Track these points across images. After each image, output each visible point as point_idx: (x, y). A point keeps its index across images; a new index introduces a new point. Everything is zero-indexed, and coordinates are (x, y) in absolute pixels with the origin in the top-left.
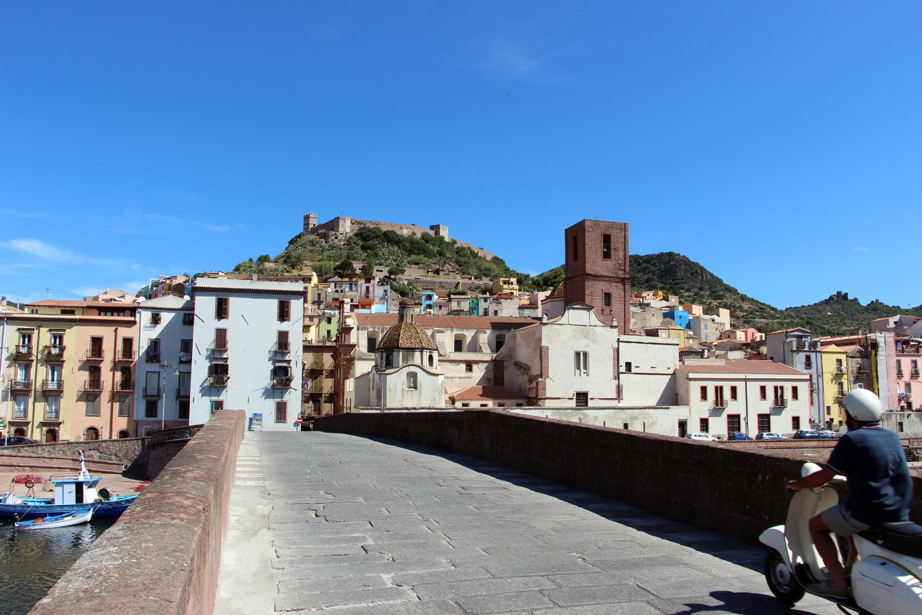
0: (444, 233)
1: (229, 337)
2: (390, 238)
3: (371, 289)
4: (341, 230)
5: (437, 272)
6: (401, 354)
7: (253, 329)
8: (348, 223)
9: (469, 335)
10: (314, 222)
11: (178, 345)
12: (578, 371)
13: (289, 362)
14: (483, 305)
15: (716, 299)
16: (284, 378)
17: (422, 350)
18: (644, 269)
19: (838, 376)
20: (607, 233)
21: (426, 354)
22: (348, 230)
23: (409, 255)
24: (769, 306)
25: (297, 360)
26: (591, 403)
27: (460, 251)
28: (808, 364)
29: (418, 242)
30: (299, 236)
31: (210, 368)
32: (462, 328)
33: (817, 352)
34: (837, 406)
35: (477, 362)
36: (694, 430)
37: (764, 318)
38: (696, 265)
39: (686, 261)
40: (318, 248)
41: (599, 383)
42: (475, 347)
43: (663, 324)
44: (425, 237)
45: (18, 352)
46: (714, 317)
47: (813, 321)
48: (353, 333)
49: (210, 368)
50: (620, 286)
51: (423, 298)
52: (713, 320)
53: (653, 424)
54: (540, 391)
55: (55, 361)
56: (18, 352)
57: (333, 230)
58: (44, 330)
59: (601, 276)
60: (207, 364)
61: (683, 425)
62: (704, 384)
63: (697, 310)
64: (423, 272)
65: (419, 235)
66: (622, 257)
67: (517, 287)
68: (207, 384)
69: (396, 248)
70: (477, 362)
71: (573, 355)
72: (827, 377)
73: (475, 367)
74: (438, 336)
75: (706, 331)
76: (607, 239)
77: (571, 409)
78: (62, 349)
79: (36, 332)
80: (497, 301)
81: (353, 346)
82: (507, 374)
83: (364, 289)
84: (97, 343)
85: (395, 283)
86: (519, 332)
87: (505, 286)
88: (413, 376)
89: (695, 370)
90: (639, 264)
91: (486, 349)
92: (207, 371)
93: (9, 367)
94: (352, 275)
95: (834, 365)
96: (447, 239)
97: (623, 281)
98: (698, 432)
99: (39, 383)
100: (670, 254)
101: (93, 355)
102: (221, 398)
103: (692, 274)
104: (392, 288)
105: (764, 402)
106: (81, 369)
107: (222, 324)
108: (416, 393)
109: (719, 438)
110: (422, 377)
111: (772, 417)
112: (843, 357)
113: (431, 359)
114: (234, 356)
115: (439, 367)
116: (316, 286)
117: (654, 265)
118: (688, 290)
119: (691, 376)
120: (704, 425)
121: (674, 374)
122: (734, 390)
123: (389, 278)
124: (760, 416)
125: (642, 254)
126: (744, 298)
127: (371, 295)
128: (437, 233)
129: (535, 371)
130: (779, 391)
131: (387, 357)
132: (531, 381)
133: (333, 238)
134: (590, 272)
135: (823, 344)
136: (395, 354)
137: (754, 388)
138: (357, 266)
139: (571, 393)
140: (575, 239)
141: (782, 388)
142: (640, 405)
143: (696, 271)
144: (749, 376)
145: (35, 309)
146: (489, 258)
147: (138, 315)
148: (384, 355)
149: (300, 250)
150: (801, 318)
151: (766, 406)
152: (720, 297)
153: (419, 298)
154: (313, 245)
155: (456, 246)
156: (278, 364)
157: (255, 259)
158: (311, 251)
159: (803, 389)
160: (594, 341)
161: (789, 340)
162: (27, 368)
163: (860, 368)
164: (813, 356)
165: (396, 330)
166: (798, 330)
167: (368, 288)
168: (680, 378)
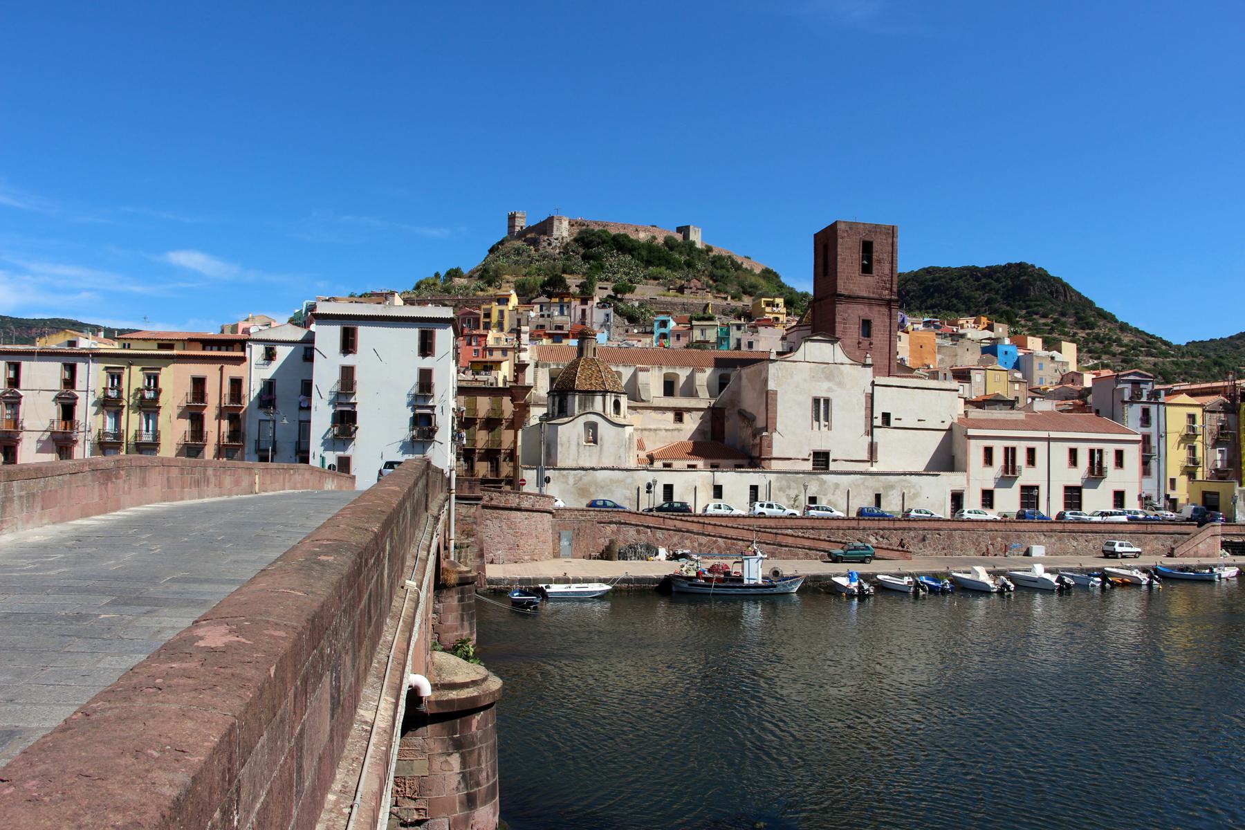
0: (696, 237)
1: (358, 376)
2: (622, 244)
3: (588, 312)
4: (556, 233)
5: (681, 290)
6: (577, 398)
7: (387, 366)
8: (565, 224)
9: (683, 374)
10: (521, 223)
11: (298, 387)
12: (816, 424)
13: (433, 408)
14: (735, 334)
15: (1083, 328)
16: (426, 428)
17: (604, 393)
18: (984, 287)
19: (1188, 438)
20: (868, 239)
21: (610, 400)
22: (565, 234)
23: (646, 267)
24: (1160, 340)
25: (446, 404)
26: (832, 466)
27: (718, 262)
28: (1146, 419)
29: (658, 250)
30: (501, 243)
31: (334, 415)
32: (674, 366)
33: (1159, 404)
34: (1185, 478)
35: (689, 410)
36: (972, 502)
37: (1152, 356)
38: (1058, 280)
39: (1043, 276)
40: (524, 257)
41: (844, 438)
42: (690, 390)
43: (980, 362)
44: (669, 243)
45: (106, 396)
46: (1054, 353)
47: (1224, 361)
48: (529, 372)
49: (335, 416)
50: (884, 310)
51: (656, 324)
52: (1053, 358)
53: (916, 495)
54: (765, 449)
55: (149, 407)
56: (106, 396)
57: (545, 233)
58: (136, 369)
59: (858, 297)
60: (330, 410)
61: (957, 499)
62: (988, 443)
63: (1035, 344)
64: (661, 290)
65: (660, 240)
66: (887, 271)
67: (784, 310)
68: (330, 435)
69: (628, 258)
70: (689, 410)
71: (810, 402)
72: (1173, 439)
73: (686, 416)
74: (641, 375)
75: (1041, 373)
76: (867, 247)
77: (804, 473)
78: (158, 392)
79: (127, 371)
80: (754, 329)
81: (529, 388)
82: (729, 426)
83: (579, 313)
84: (199, 383)
85: (621, 305)
86: (746, 372)
87: (768, 309)
88: (592, 427)
89: (978, 424)
90: (978, 279)
91: (704, 393)
92: (330, 419)
93: (96, 414)
94: (565, 294)
95: (1184, 422)
96: (699, 245)
97: (889, 304)
98: (978, 507)
99: (131, 434)
100: (1021, 266)
101: (195, 399)
102: (347, 453)
103: (1051, 293)
104: (616, 311)
105: (1073, 470)
106: (180, 416)
107: (349, 360)
108: (596, 448)
109: (1005, 516)
110: (604, 428)
111: (1084, 491)
112: (1198, 412)
113: (617, 405)
114: (363, 400)
115: (628, 416)
116: (516, 309)
117: (998, 280)
118: (1044, 316)
119: (971, 432)
120: (988, 498)
121: (950, 430)
122: (1031, 453)
123: (614, 298)
124: (1067, 488)
125: (982, 264)
126: (1124, 327)
127: (588, 321)
128: (686, 237)
129: (760, 423)
130: (1097, 455)
131: (561, 402)
132: (754, 436)
133: (545, 244)
134: (843, 292)
135: (1169, 393)
136: (570, 398)
137: (1060, 452)
138: (573, 282)
139: (806, 452)
140: (826, 247)
141: (1100, 451)
142: (901, 470)
143: (1057, 289)
144: (1054, 435)
145: (127, 342)
146: (757, 271)
147: (248, 350)
148: (557, 399)
149: (502, 262)
150: (1207, 357)
151: (1076, 476)
152: (1091, 326)
153: (652, 325)
154: (518, 254)
155: (711, 254)
156: (418, 411)
157: (443, 274)
158: (516, 263)
159: (1133, 455)
160: (840, 384)
161: (1120, 386)
162: (117, 415)
163: (1222, 427)
164: (1153, 409)
165: (574, 366)
166: (1135, 374)
167: (584, 311)
168: (957, 434)
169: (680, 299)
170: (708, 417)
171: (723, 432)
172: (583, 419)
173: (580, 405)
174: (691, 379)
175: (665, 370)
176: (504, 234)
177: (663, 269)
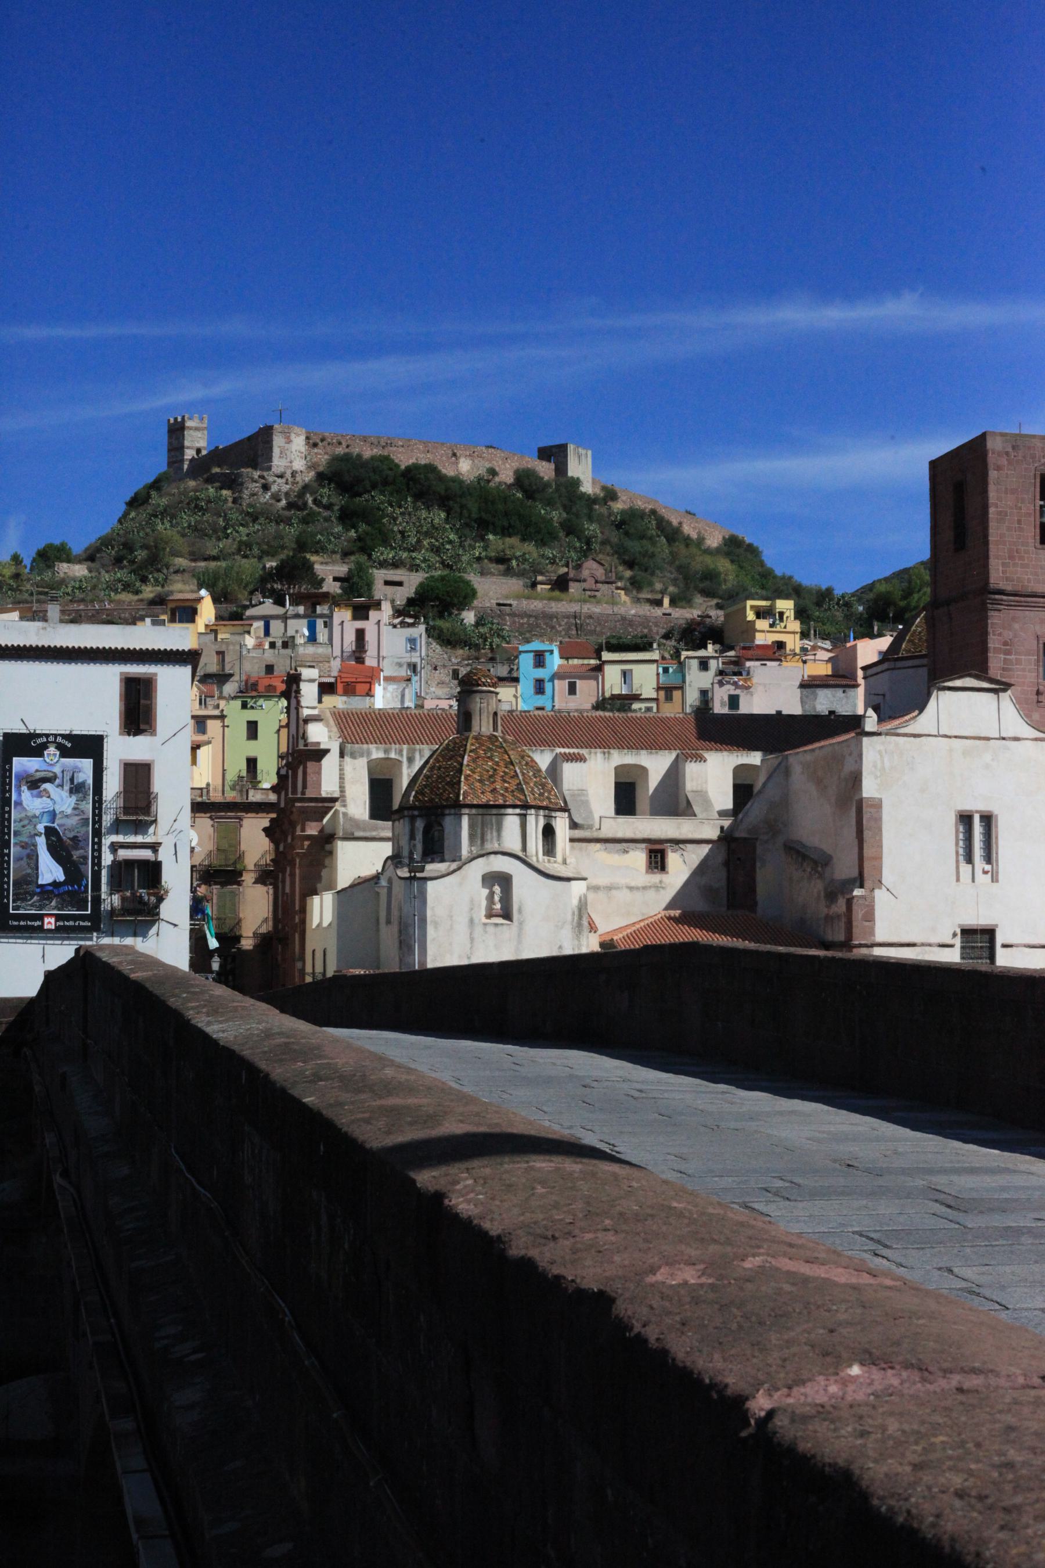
0: (581, 468)
2: (422, 485)
3: (370, 637)
4: (278, 463)
5: (561, 584)
6: (465, 822)
10: (197, 441)
12: (965, 869)
13: (154, 847)
21: (535, 823)
22: (299, 465)
29: (502, 495)
30: (156, 485)
44: (525, 480)
67: (795, 626)
69: (439, 516)
70: (678, 842)
71: (951, 820)
75: (252, 749)
83: (350, 638)
87: (762, 624)
96: (587, 488)
110: (526, 886)
113: (549, 832)
128: (561, 469)
129: (844, 868)
132: (831, 896)
133: (255, 487)
136: (448, 822)
138: (329, 571)
146: (714, 541)
167: (360, 634)
169: (563, 606)
170: (721, 858)
171: (752, 890)
172: (478, 869)
173: (472, 837)
174: (674, 776)
175: (377, 753)
176: (158, 464)
177: (514, 541)
